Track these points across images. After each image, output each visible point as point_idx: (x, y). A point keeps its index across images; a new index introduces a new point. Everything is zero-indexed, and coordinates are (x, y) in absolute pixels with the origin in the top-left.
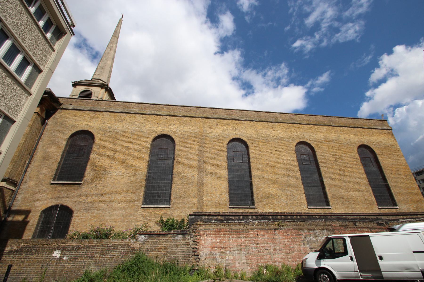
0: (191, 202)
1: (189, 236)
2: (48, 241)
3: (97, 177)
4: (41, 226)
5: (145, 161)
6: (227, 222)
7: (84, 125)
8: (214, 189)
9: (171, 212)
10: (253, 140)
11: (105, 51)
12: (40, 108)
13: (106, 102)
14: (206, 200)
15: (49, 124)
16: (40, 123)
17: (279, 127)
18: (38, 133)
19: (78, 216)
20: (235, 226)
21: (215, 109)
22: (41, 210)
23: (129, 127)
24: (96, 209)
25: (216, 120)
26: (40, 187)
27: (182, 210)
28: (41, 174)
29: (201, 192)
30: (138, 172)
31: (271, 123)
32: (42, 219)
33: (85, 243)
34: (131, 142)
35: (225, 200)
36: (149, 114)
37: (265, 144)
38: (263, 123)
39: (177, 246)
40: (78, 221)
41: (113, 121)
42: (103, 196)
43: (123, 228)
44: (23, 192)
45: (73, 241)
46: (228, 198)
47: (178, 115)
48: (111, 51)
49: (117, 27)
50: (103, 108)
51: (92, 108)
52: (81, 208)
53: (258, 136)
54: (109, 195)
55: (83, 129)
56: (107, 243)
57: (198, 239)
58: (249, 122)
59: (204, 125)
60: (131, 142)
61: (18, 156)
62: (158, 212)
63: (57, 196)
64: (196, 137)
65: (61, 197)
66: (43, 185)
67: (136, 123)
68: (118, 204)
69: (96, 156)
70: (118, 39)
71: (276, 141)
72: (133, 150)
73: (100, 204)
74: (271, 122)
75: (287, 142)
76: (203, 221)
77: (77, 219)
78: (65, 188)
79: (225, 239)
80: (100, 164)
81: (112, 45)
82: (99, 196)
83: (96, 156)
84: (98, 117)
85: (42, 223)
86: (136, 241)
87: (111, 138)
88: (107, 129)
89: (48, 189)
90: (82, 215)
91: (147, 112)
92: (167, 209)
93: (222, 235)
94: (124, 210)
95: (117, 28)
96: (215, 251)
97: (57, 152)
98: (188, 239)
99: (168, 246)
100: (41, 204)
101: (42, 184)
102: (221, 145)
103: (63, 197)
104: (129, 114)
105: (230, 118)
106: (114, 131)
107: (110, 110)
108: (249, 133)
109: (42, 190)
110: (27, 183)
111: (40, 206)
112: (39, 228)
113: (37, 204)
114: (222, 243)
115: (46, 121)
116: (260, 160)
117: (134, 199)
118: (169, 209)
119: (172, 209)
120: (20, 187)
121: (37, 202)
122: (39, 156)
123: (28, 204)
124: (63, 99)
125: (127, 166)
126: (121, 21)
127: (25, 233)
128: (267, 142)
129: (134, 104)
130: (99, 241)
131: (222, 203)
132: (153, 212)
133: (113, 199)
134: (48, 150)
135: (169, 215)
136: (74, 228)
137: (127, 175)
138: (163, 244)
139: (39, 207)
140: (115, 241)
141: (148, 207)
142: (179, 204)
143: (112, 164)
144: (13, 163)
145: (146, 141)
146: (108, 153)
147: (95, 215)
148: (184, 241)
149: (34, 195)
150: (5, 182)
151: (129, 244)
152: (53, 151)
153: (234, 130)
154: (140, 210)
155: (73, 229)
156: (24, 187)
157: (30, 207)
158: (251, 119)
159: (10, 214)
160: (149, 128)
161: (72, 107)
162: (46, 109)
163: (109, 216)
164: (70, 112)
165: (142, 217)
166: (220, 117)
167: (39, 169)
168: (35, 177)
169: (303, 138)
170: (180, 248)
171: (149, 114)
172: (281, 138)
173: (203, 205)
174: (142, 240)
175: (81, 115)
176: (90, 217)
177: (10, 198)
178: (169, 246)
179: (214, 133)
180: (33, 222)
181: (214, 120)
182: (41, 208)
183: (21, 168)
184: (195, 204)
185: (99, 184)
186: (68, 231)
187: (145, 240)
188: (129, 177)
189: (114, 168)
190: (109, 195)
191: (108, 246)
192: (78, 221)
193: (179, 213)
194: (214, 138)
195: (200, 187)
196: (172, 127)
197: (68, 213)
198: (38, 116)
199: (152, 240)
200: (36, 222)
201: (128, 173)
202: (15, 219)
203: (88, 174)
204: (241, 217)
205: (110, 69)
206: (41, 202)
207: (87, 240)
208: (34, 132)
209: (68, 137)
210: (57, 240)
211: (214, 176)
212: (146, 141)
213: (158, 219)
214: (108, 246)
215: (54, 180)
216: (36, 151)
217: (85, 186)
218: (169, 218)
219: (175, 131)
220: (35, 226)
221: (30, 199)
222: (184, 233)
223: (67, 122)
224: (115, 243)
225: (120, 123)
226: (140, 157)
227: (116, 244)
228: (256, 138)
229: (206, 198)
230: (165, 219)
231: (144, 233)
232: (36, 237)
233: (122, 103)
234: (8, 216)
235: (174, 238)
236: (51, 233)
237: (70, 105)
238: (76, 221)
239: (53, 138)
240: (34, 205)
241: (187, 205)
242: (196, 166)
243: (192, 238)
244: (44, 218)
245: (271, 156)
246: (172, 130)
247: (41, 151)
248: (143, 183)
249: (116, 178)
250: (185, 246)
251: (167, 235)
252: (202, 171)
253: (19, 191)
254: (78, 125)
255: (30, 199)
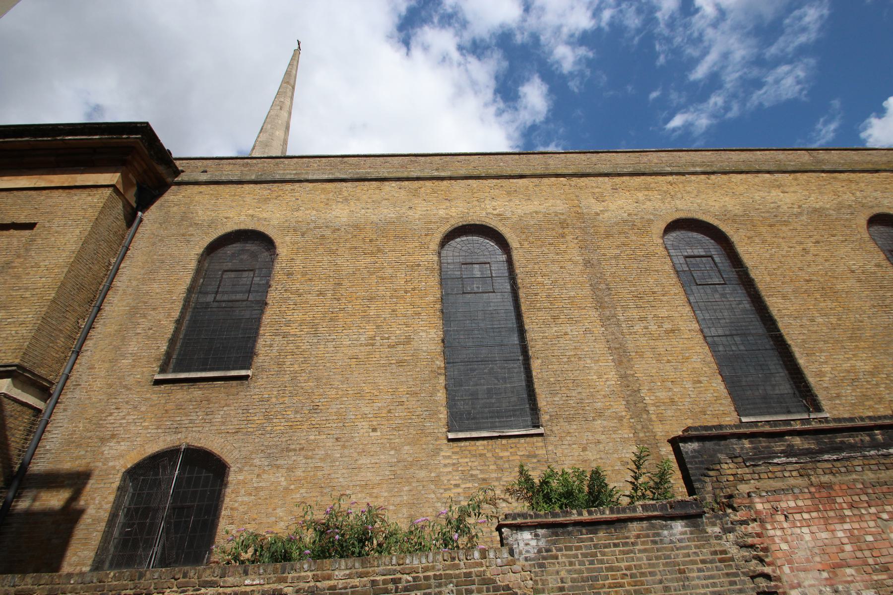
0: (608, 413)
1: (714, 525)
2: (140, 578)
3: (293, 353)
4: (124, 525)
5: (430, 298)
6: (835, 457)
7: (243, 218)
8: (668, 367)
9: (550, 448)
10: (734, 221)
11: (269, 112)
12: (121, 175)
13: (296, 159)
14: (653, 405)
15: (147, 222)
16: (123, 217)
17: (795, 183)
18: (116, 246)
19: (244, 482)
20: (870, 469)
21: (595, 155)
22: (124, 470)
23: (367, 213)
24: (303, 453)
25: (606, 179)
26: (121, 396)
27: (585, 442)
28: (124, 356)
29: (630, 379)
30: (415, 332)
31: (768, 175)
32: (127, 499)
33: (299, 578)
34: (379, 250)
35: (717, 398)
36: (418, 179)
37: (775, 229)
38: (743, 176)
39: (682, 572)
40: (246, 499)
41: (322, 202)
42: (319, 411)
43: (400, 515)
44: (69, 413)
45: (246, 573)
46: (725, 391)
47: (499, 173)
48: (282, 112)
49: (289, 64)
50: (291, 174)
51: (261, 175)
52: (252, 453)
53: (745, 211)
54: (338, 406)
55: (242, 227)
56: (394, 572)
57: (759, 535)
58: (703, 177)
59: (577, 194)
60: (379, 250)
61: (54, 301)
62: (506, 454)
63: (172, 419)
64: (563, 224)
65: (187, 422)
66: (130, 389)
67: (384, 202)
68: (372, 434)
69: (286, 295)
70: (293, 88)
71: (804, 218)
72: (390, 271)
73: (312, 437)
74: (769, 172)
75: (836, 219)
76: (740, 460)
77: (242, 492)
78: (197, 392)
79: (864, 525)
80: (298, 316)
81: (282, 100)
82: (307, 412)
83: (286, 295)
84: (280, 196)
85: (129, 513)
86: (510, 558)
87: (321, 244)
88: (308, 224)
89: (146, 399)
90: (258, 476)
91: (413, 173)
92: (535, 439)
93: (848, 512)
94: (392, 452)
95: (290, 67)
96: (849, 582)
97: (170, 292)
98: (718, 538)
99: (643, 574)
100: (123, 448)
101: (125, 387)
102: (647, 239)
103: (191, 422)
104: (362, 183)
105: (647, 171)
106: (327, 227)
107: (310, 177)
108: (717, 205)
109: (127, 403)
110: (80, 385)
111: (121, 456)
112: (116, 532)
113: (111, 448)
114: (864, 546)
115: (140, 214)
116: (779, 272)
117: (417, 413)
118: (540, 439)
119: (552, 438)
120: (58, 398)
121: (112, 444)
122: (119, 307)
123: (83, 453)
124: (184, 161)
125: (378, 316)
126: (289, 80)
127: (69, 553)
128: (777, 221)
129: (371, 158)
130: (357, 565)
131: (710, 409)
132: (489, 455)
133: (353, 417)
134: (145, 288)
135: (546, 462)
136: (232, 524)
137: (384, 341)
138: (623, 565)
139: (115, 458)
140: (424, 560)
141: (469, 436)
142: (569, 420)
143: (332, 313)
144: (39, 322)
145: (423, 246)
146: (319, 286)
147: (299, 473)
148: (703, 546)
149: (101, 422)
150: (10, 380)
151: (488, 574)
152: (157, 291)
153: (669, 199)
154: (444, 447)
155: (229, 528)
156: (72, 398)
157: (88, 460)
158: (708, 169)
159: (24, 488)
160: (424, 211)
161: (209, 176)
162: (137, 182)
163: (346, 475)
164: (202, 190)
165: (457, 471)
166: (619, 170)
167: (119, 341)
168: (107, 365)
169: (877, 206)
170: (699, 578)
171: (418, 179)
172: (815, 210)
173: (650, 420)
174: (527, 552)
175: (234, 195)
176: (284, 484)
177: (28, 435)
178: (652, 574)
179: (613, 211)
180: (97, 512)
181: (600, 179)
182: (122, 462)
183: (63, 340)
184: (621, 419)
185: (304, 374)
186: (214, 538)
187: (540, 551)
188: (389, 346)
189: (341, 323)
190: (338, 406)
191: (397, 588)
192: (246, 499)
193: (576, 451)
194: (617, 224)
195: (621, 362)
196: (489, 205)
197: (212, 475)
198: (114, 195)
199: (569, 548)
200: (106, 510)
201: (387, 336)
202: (37, 506)
203: (265, 346)
204: (879, 435)
205: (281, 147)
206: (122, 443)
207: (306, 566)
208: (105, 241)
209: (201, 251)
210: (180, 571)
211: (653, 328)
212: (423, 246)
213: (512, 477)
214: (400, 586)
215: (163, 370)
216: (110, 292)
217: (260, 382)
218: (548, 470)
219: (500, 215)
220: (104, 524)
221: (89, 434)
222: (692, 511)
223: (197, 213)
224: (425, 569)
225: (340, 206)
226: (414, 289)
227: (431, 574)
228: (741, 214)
229: (653, 398)
230: (536, 477)
231: (529, 520)
232: (107, 564)
233: (338, 159)
234: (18, 496)
235: (658, 535)
236: (157, 549)
237: (203, 172)
238: (240, 499)
239: (160, 255)
240: (102, 453)
241: (596, 423)
242: (589, 302)
243: (731, 530)
244: (133, 495)
245: (809, 258)
246: (490, 213)
247: (124, 292)
248: (438, 363)
249: (350, 352)
250: (718, 569)
251: (623, 525)
252: (614, 316)
253: (55, 411)
254: (226, 218)
255: (89, 434)
